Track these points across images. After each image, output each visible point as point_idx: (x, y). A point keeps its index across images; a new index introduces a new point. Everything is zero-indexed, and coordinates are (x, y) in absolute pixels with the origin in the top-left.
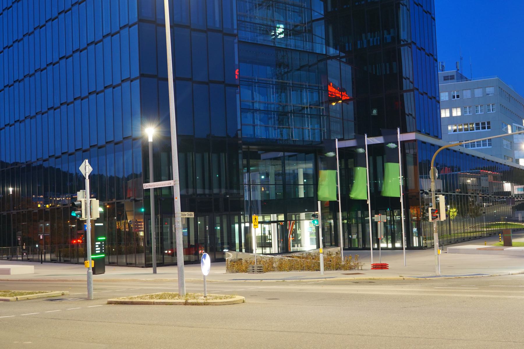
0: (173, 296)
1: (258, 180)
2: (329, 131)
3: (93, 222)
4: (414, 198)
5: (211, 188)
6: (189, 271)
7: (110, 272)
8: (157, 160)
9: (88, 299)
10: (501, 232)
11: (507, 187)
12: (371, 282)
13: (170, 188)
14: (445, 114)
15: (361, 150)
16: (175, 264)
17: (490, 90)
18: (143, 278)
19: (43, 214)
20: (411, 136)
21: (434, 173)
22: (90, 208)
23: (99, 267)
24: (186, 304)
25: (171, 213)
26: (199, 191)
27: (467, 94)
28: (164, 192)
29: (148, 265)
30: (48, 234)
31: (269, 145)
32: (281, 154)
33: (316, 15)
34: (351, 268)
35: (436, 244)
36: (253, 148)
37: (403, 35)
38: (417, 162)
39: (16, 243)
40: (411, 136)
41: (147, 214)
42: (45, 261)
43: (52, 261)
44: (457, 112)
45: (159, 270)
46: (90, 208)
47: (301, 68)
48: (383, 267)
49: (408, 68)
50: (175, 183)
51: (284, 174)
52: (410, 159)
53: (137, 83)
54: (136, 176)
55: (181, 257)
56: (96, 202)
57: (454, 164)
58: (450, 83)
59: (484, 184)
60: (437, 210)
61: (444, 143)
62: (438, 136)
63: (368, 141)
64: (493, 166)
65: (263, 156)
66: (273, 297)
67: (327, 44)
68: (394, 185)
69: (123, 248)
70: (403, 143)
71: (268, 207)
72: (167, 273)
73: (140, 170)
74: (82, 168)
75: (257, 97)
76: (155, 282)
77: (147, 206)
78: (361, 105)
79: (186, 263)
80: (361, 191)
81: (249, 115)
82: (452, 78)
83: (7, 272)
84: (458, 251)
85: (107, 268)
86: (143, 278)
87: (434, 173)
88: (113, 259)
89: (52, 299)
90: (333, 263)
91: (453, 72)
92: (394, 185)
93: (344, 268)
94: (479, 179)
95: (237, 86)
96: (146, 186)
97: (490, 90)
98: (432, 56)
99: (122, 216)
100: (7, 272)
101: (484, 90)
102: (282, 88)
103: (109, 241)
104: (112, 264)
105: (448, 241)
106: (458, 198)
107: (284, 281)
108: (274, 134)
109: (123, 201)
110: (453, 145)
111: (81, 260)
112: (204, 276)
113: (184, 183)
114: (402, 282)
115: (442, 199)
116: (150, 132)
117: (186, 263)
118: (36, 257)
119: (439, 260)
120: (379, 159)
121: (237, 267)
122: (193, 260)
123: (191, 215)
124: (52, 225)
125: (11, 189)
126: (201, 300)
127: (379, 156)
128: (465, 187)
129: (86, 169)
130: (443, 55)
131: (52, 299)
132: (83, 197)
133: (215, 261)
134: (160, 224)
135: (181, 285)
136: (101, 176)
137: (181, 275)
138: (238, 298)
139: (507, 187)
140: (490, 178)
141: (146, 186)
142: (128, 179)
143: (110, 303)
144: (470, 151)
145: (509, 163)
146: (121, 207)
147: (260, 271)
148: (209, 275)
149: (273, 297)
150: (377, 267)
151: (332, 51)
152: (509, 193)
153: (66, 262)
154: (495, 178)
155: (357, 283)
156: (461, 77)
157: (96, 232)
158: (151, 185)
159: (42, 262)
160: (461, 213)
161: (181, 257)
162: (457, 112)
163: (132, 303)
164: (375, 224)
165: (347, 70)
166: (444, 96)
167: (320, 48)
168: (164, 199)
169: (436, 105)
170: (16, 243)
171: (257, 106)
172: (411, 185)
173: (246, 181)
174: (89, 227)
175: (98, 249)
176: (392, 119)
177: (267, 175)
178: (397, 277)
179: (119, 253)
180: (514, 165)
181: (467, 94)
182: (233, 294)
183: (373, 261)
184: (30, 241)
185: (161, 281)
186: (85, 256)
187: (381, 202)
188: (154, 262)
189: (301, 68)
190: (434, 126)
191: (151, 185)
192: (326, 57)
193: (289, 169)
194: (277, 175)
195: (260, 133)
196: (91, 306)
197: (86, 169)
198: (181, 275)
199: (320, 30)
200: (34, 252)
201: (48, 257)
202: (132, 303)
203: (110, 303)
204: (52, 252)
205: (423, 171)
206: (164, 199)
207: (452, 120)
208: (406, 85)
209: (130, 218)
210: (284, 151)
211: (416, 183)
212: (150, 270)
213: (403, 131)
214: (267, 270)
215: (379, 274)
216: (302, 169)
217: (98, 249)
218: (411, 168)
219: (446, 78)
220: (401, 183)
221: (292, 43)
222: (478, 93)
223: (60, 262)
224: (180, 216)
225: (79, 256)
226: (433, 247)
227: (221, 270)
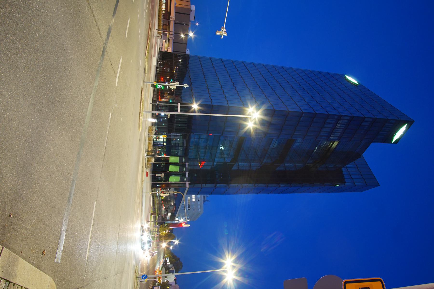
0: (143, 109)
1: (177, 138)
2: (191, 161)
3: (169, 86)
4: (168, 186)
5: (176, 123)
6: (150, 114)
7: (152, 89)
8: (186, 109)
9: (144, 82)
10: (155, 212)
11: (169, 214)
12: (143, 171)
13: (177, 111)
14: (194, 196)
15: (184, 170)
16: (153, 110)
17: (200, 210)
18: (149, 100)
19: (172, 70)
20: (188, 186)
21: (176, 193)
22: (174, 85)
23: (154, 86)
24: (140, 113)
25: (169, 111)
26: (175, 120)
27: (199, 203)
28: (176, 109)
29: (153, 101)
30: (166, 71)
31: (188, 142)
32: (185, 146)
33: (226, 159)
34: (147, 165)
35: (153, 192)
36: (187, 138)
37: (218, 185)
38: (180, 187)
39: (163, 60)
40: (188, 186)
41: (170, 103)
42: (157, 69)
43: (157, 71)
44: (194, 200)
45: (151, 105)
46: (174, 85)
47: (211, 154)
48: (147, 175)
49: (208, 186)
50: (179, 113)
51: (179, 146)
52: (181, 185)
53: (210, 104)
54: (181, 100)
55: (157, 113)
56: (175, 88)
57: (178, 199)
58: (203, 198)
59: (171, 208)
60: (164, 193)
61: (184, 196)
62: (187, 194)
63: (187, 173)
64: (176, 210)
65: (185, 140)
66: (140, 141)
67: (217, 162)
68: (173, 180)
69: (159, 93)
70: (186, 183)
71: (169, 140)
72: (150, 107)
73: (183, 102)
74: (186, 84)
75: (203, 140)
76: (148, 103)
77: (172, 103)
78: (198, 171)
79: (153, 114)
80: (172, 169)
81: (198, 137)
82: (204, 199)
83: (154, 56)
84: (150, 197)
85: (153, 88)
86: (149, 100)
87: (176, 193)
88: (156, 90)
89: (145, 70)
90: (149, 160)
91: (206, 199)
92: (173, 180)
93: (148, 163)
94: (172, 206)
95: (207, 133)
96: (179, 104)
97: (200, 210)
98: (211, 193)
99: (169, 94)
100: (154, 56)
101: (200, 209)
102: (205, 147)
103: (162, 90)
104: (154, 90)
105: (154, 196)
106: (166, 201)
107: (145, 144)
108: (191, 144)
109: (174, 95)
110: (184, 199)
111: (156, 80)
112: (359, 155)
113: (178, 115)
114: (142, 181)
115: (167, 195)
116: (195, 106)
117: (153, 114)
118: (158, 66)
119: (147, 192)
120: (181, 176)
121: (150, 130)
122: (153, 116)
123: (169, 117)
124: (168, 72)
125: (181, 61)
126: (141, 118)
127: (182, 175)
128: (170, 201)
129: (186, 86)
130: (211, 196)
131: (145, 70)
132: (177, 84)
133: (153, 124)
134: (166, 107)
135: (146, 112)
136: (182, 89)
137: (149, 112)
138: (141, 129)
139: (169, 214)
140: (173, 209)
141: (179, 104)
142: (181, 98)
143: (142, 88)
144: (182, 202)
145: (177, 215)
146: (172, 95)
147: (148, 137)
148: (148, 121)
149: (140, 141)
150: (147, 173)
151: (215, 163)
152: (167, 215)
153: (156, 75)
154: (172, 211)
155: (143, 167)
156: (204, 202)
157: (165, 86)
158: (179, 105)
159: (157, 67)
160: (162, 200)
161: (157, 113)
162: (194, 200)
163: (141, 96)
164: (161, 173)
165: (209, 168)
166: (199, 196)
167: (216, 160)
168: (174, 109)
169: (196, 194)
170: (163, 60)
171: (200, 140)
172: (172, 185)
173: (177, 134)
174: (167, 84)
175: (159, 86)
176: (193, 180)
177: (179, 141)
178: (144, 180)
179: (158, 93)
180: (176, 217)
181: (199, 203)
182: (142, 128)
183: (149, 172)
184: (163, 65)
185: (147, 105)
186: (158, 82)
187: (167, 176)
188: (154, 103)
189: (211, 154)
190: (190, 193)
191: (179, 105)
192: (214, 162)
193: (180, 148)
194: (179, 144)
195: (192, 140)
196: (142, 82)
197: (186, 86)
198: (149, 112)
199: (222, 160)
200: (160, 65)
201: (158, 70)
202: (141, 96)
203: (142, 88)
204: (159, 71)
205: (176, 189)
206: (174, 109)
207: (191, 198)
208: (203, 185)
209: (168, 97)
210: (186, 147)
211: (173, 187)
212: (151, 102)
213: (189, 184)
214: (149, 139)
215: (145, 174)
216: (180, 151)
217: (159, 86)
218: (177, 185)
219: (204, 197)
220: (173, 182)
221: (219, 152)
222: (199, 207)
223: (156, 73)
224: (169, 114)
225: (157, 79)
226: (152, 191)
227: (150, 125)
